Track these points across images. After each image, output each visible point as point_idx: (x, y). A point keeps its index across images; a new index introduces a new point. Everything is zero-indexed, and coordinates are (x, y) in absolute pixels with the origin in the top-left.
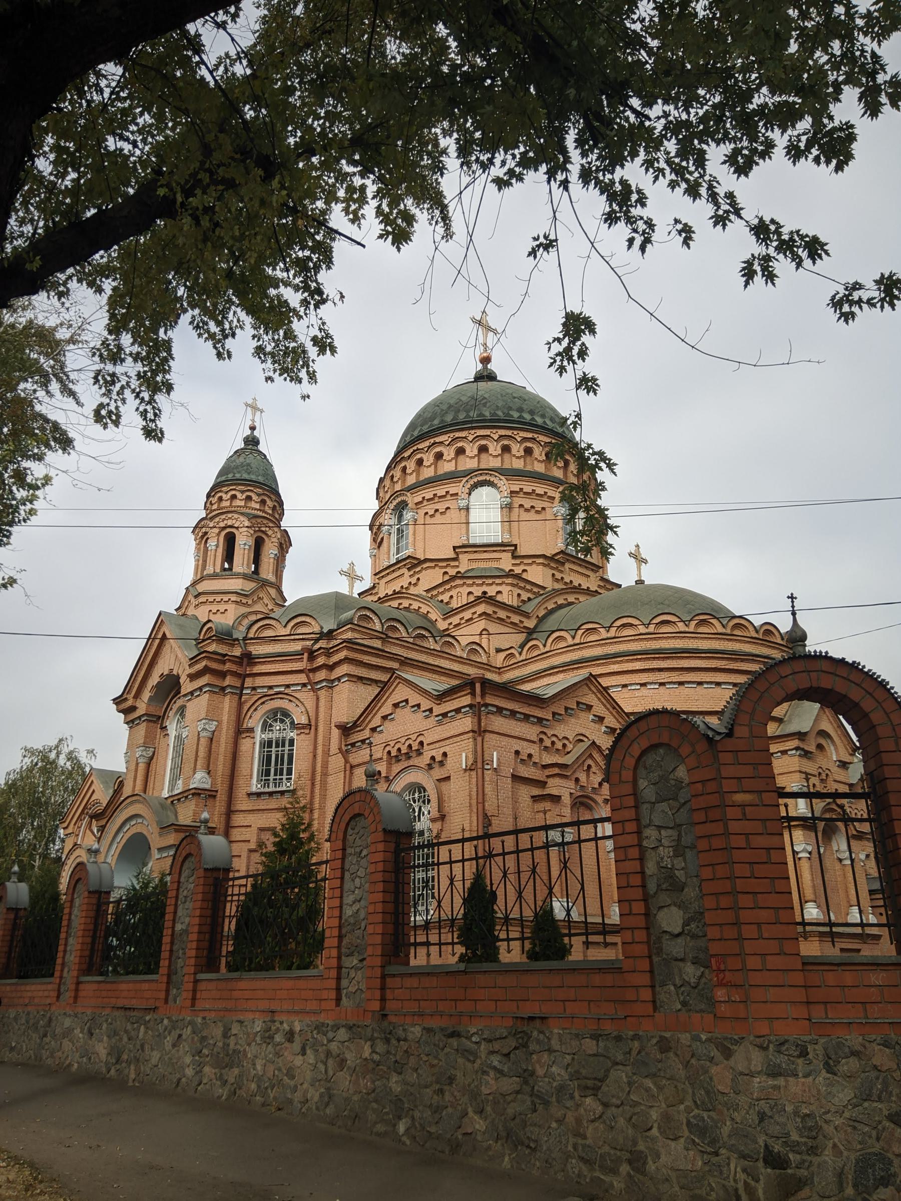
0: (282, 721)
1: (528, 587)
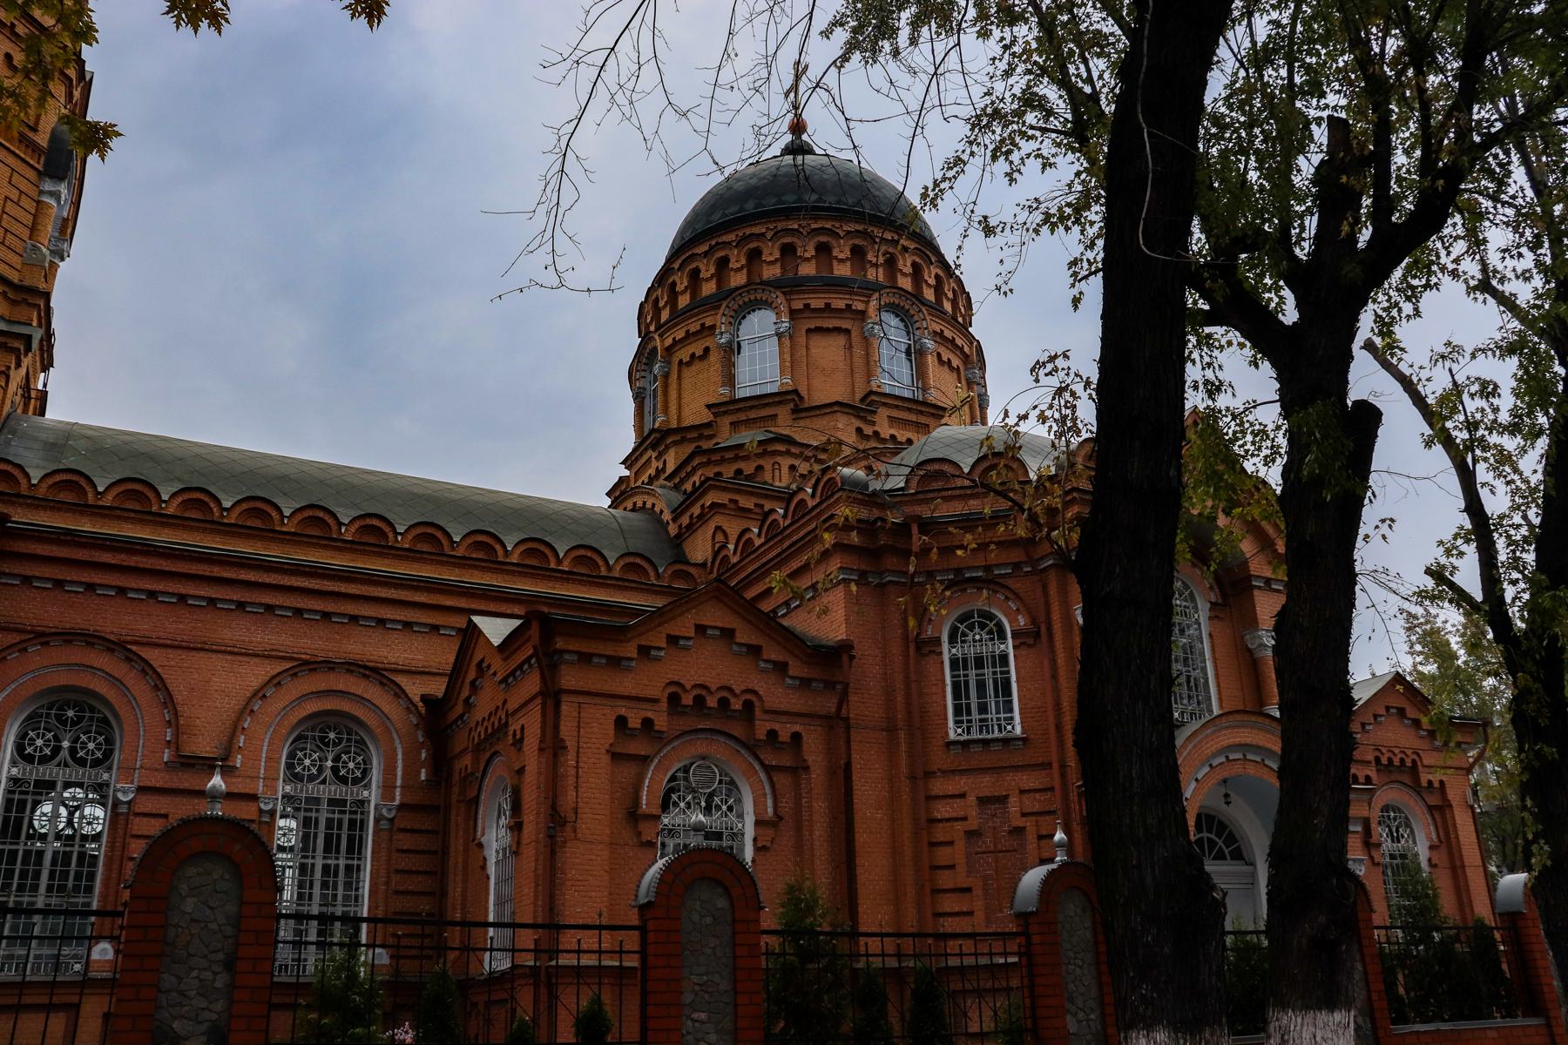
0: (982, 626)
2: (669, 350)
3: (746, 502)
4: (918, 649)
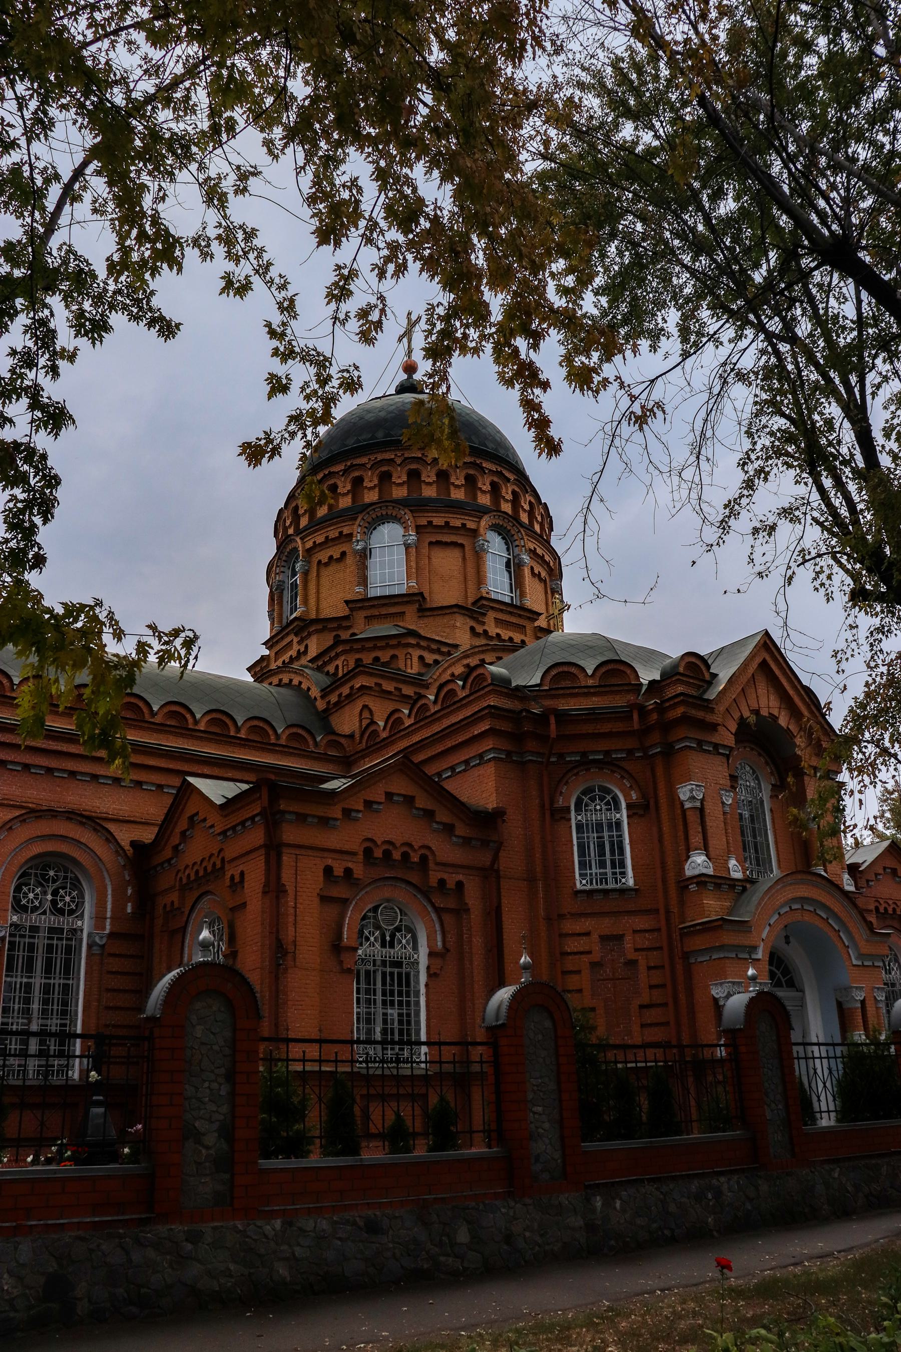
0: (602, 799)
2: (309, 551)
3: (388, 686)
4: (552, 815)
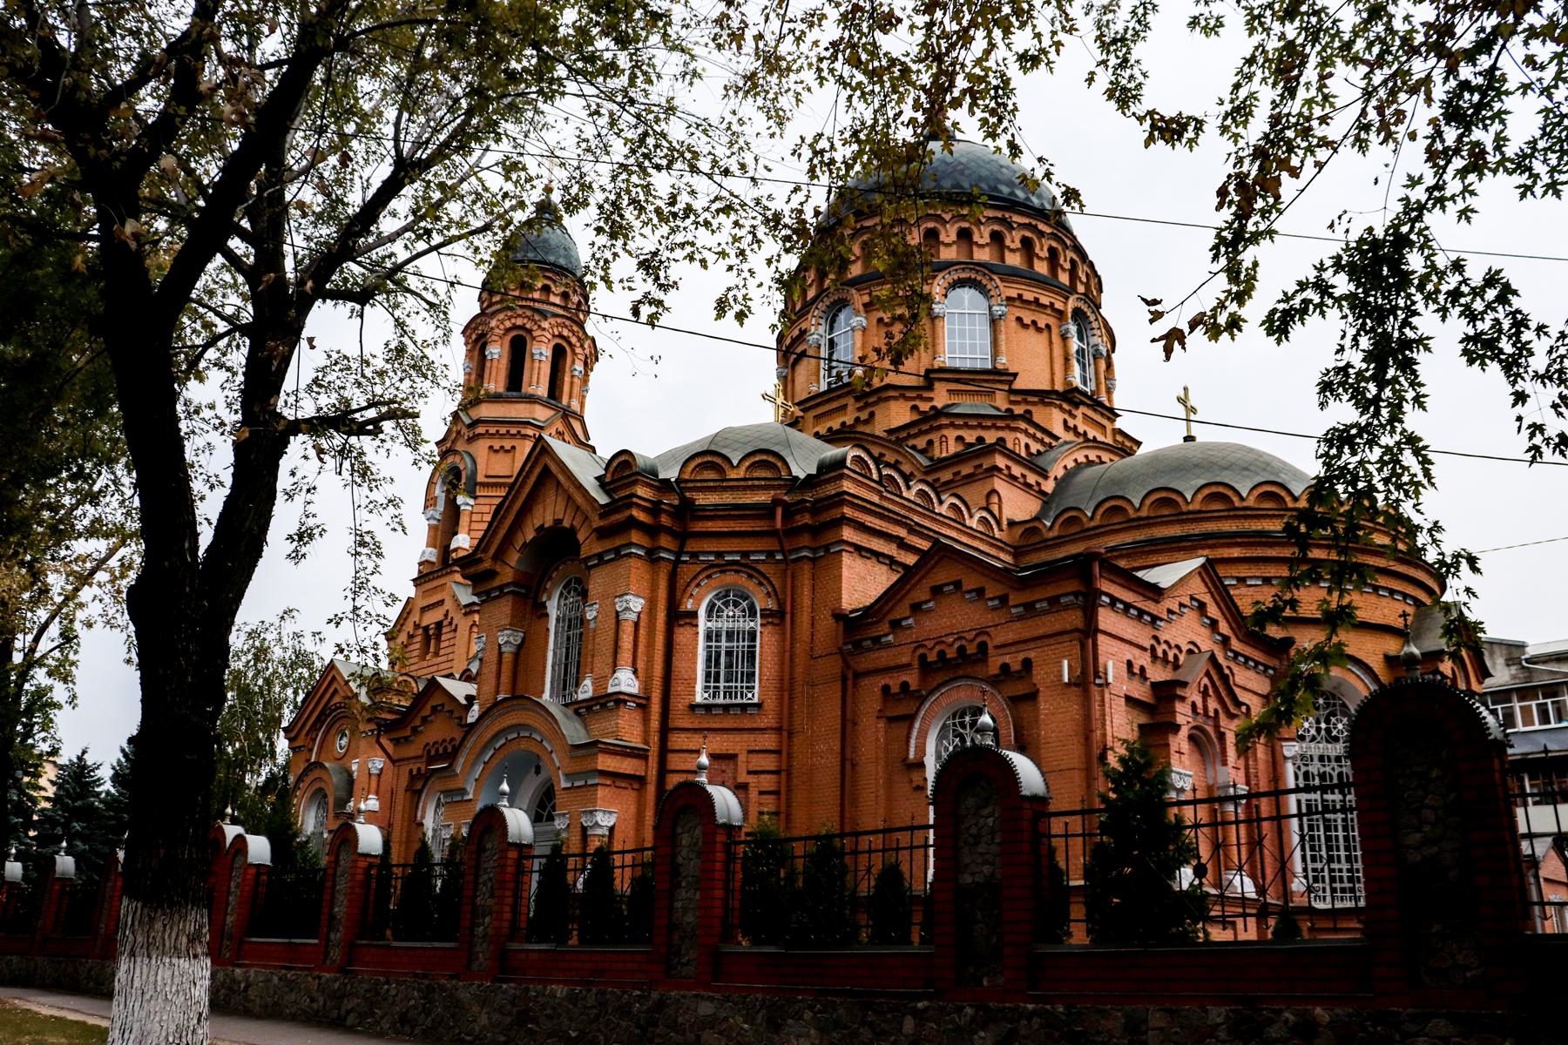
0: (736, 604)
1: (1039, 435)
